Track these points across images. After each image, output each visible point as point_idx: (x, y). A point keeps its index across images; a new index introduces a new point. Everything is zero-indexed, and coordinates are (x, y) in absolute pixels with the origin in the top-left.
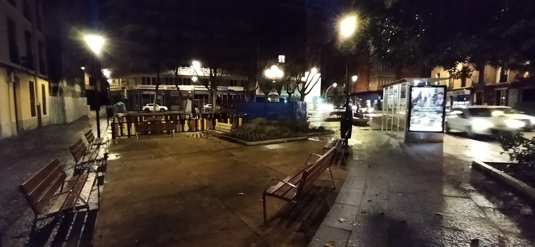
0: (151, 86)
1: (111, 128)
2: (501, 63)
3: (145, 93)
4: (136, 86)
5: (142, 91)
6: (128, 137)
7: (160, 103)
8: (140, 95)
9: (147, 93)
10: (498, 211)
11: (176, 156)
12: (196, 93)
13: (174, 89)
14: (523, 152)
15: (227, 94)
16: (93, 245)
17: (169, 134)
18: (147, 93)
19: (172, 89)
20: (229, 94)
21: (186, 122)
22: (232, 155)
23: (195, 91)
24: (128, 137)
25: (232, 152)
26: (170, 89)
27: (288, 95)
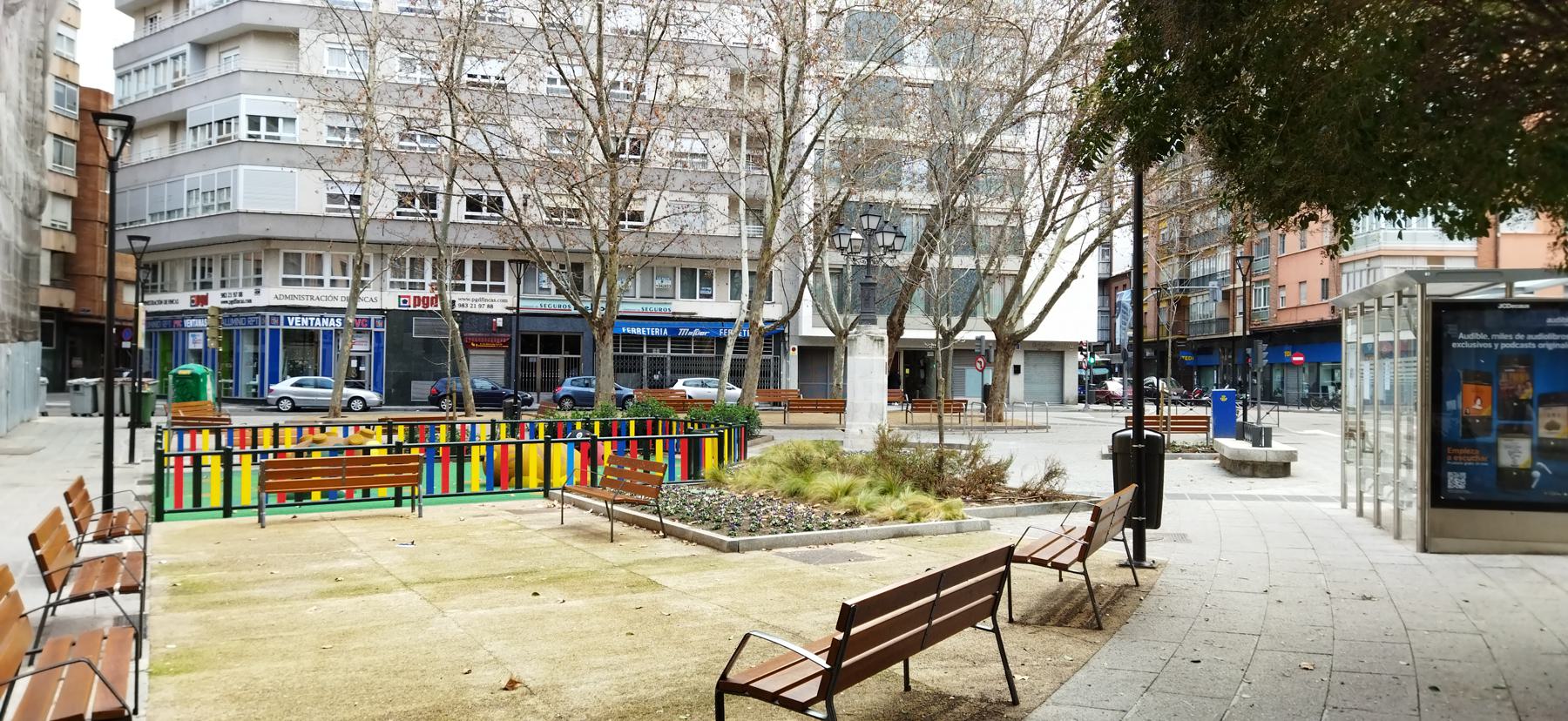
0: (326, 290)
1: (1132, 221)
2: (77, 362)
3: (298, 322)
4: (258, 292)
5: (282, 315)
6: (222, 512)
7: (361, 369)
8: (274, 333)
9: (305, 321)
10: (836, 357)
11: (429, 589)
12: (527, 326)
13: (430, 308)
14: (895, 329)
15: (666, 332)
16: (1124, 15)
17: (398, 504)
18: (305, 321)
19: (420, 308)
20: (673, 331)
21: (477, 452)
22: (653, 585)
23: (518, 315)
24: (222, 512)
25: (655, 574)
26: (412, 308)
27: (1523, 397)
